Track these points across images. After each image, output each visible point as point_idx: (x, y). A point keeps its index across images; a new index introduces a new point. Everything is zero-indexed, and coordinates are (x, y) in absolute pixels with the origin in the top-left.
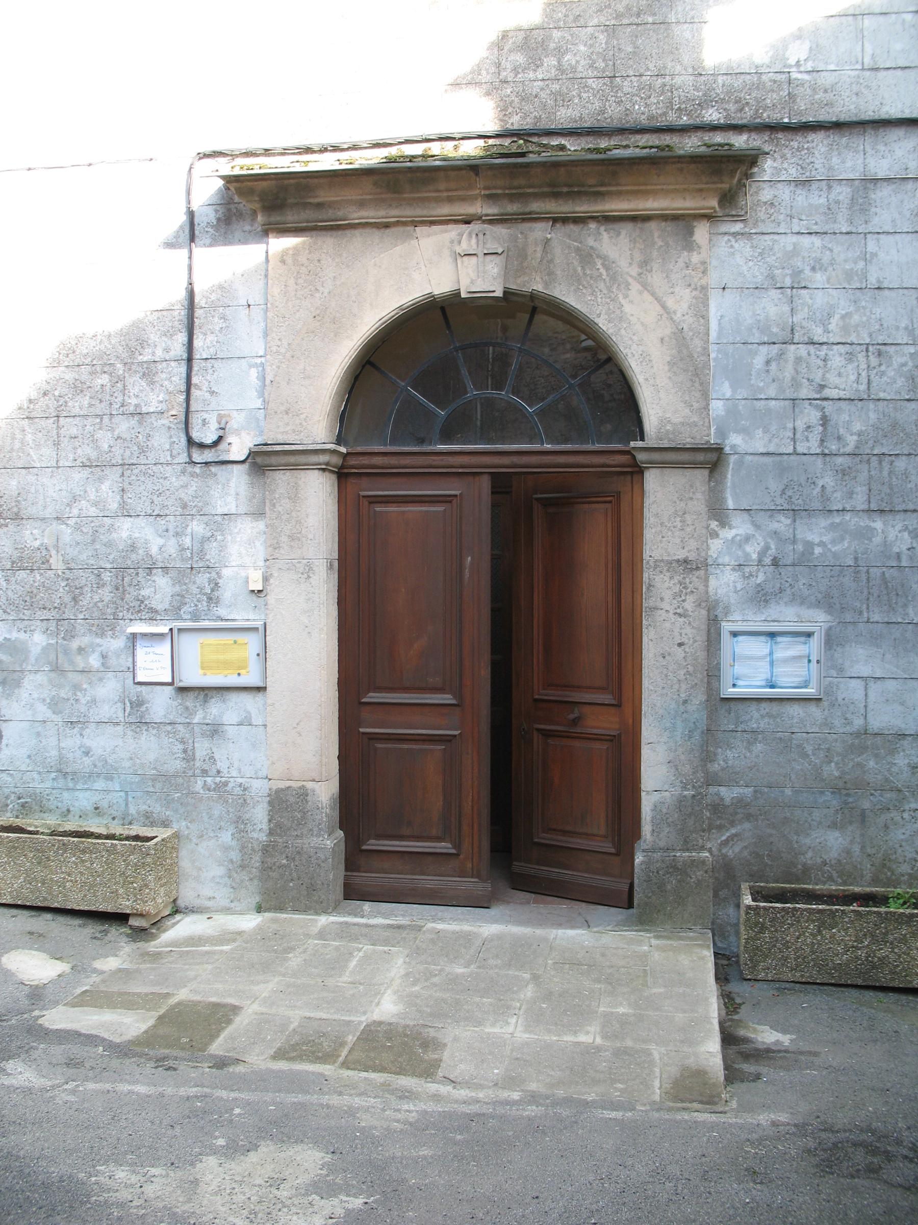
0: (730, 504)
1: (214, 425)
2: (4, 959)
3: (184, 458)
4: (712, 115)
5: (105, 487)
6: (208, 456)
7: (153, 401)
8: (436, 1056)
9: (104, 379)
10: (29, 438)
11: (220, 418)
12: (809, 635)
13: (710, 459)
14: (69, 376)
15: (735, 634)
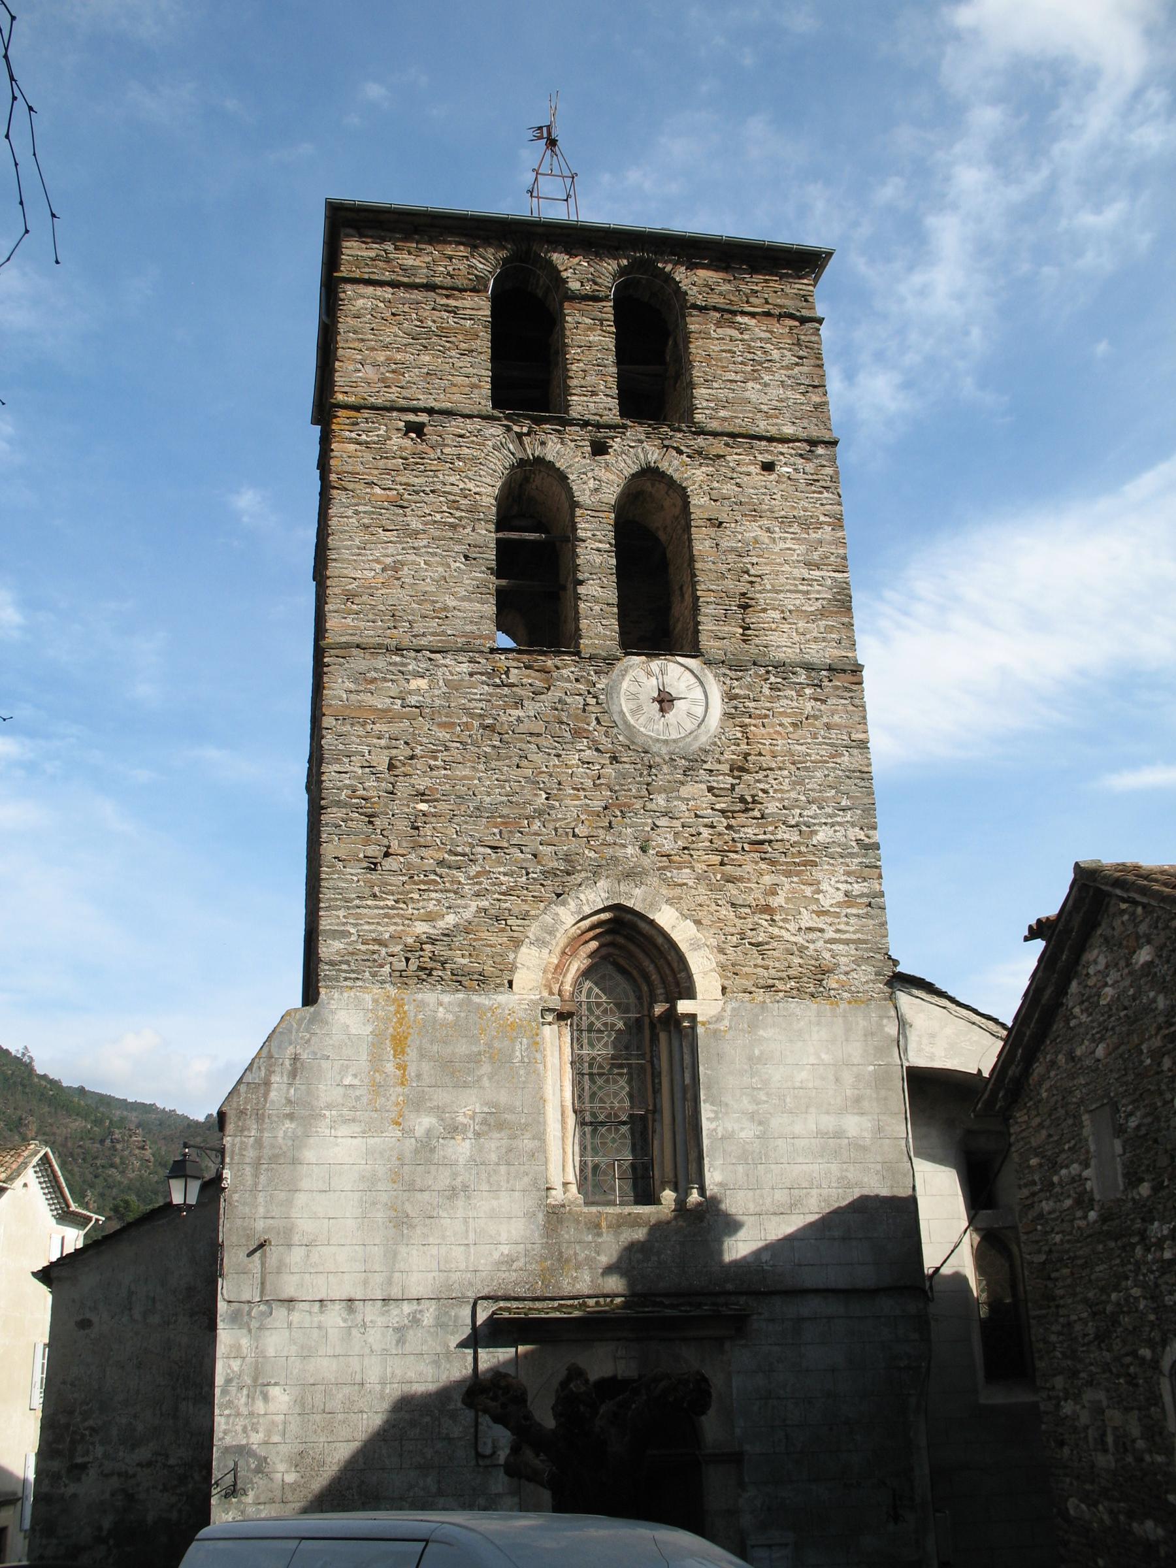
0: (747, 1480)
1: (490, 1445)
2: (1043, 943)
3: (473, 1463)
4: (729, 1287)
5: (429, 1480)
6: (488, 1462)
7: (456, 1432)
8: (371, 1141)
9: (427, 1419)
10: (384, 1451)
11: (493, 1442)
12: (786, 1545)
13: (735, 1459)
14: (407, 1416)
15: (753, 1547)
